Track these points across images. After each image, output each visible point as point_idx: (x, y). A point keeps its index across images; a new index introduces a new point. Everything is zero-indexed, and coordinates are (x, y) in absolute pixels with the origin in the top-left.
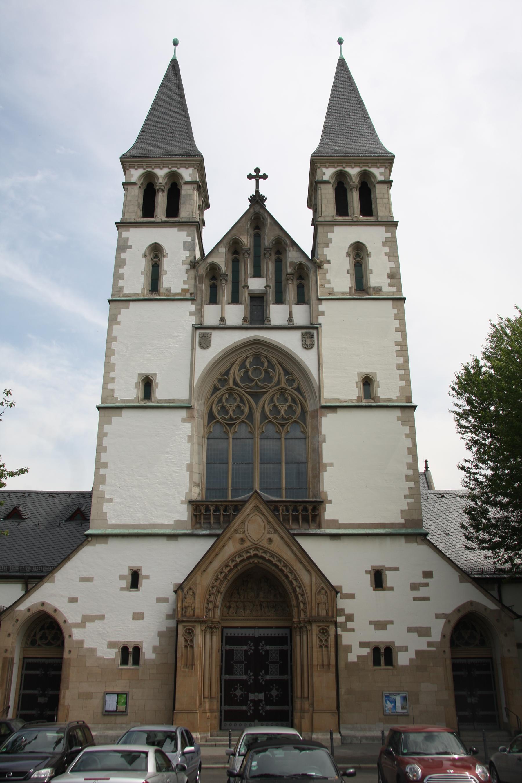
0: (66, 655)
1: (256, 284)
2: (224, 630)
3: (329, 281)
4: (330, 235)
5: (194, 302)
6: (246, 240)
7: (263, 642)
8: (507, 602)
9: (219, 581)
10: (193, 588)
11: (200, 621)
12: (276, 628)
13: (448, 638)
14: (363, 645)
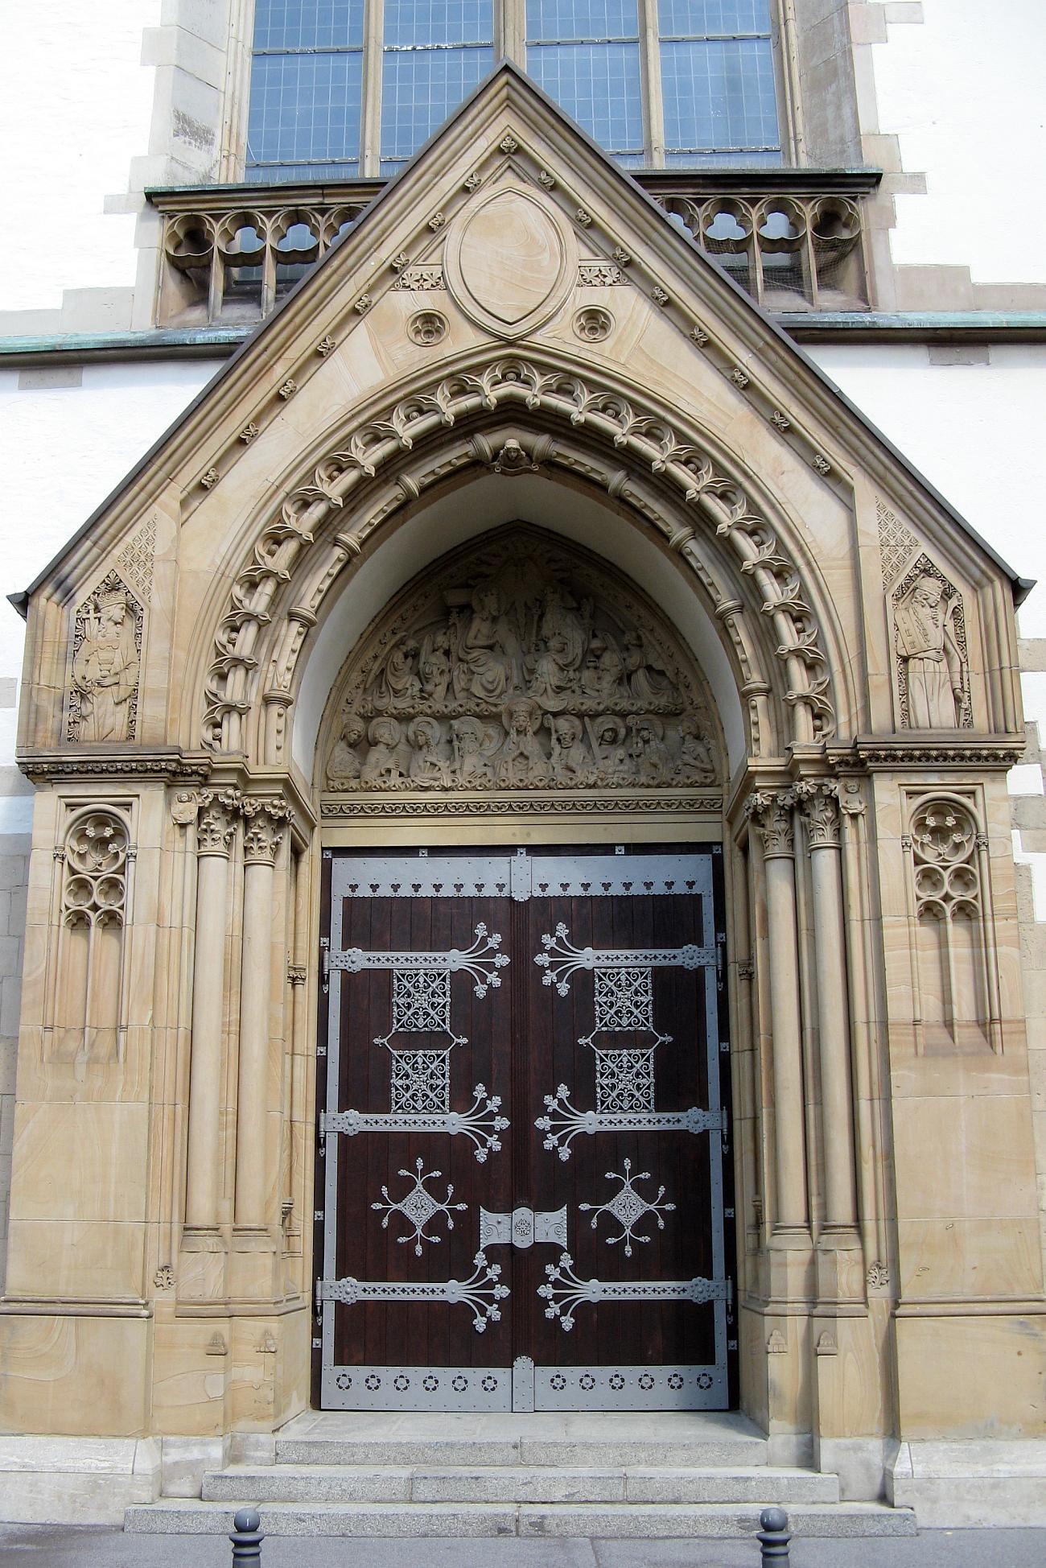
2: (339, 863)
7: (562, 930)
9: (290, 548)
10: (129, 581)
11: (175, 773)
12: (634, 849)
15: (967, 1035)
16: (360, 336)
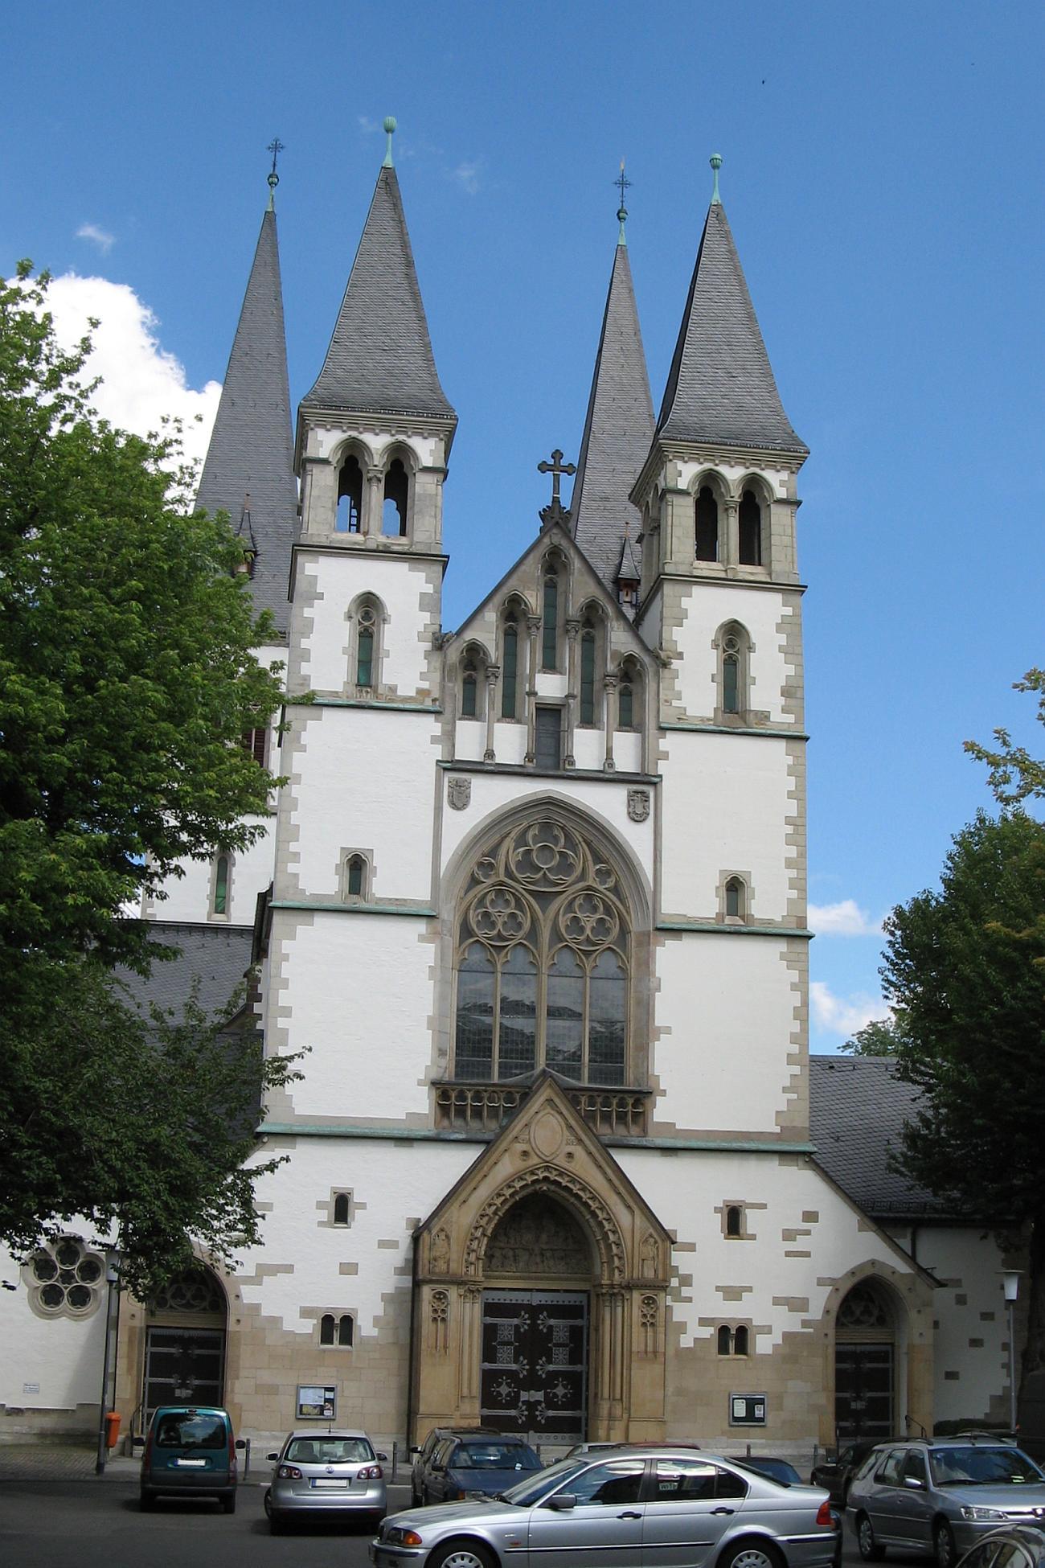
0: (232, 1326)
1: (550, 687)
3: (680, 693)
4: (685, 602)
5: (441, 717)
6: (534, 600)
8: (923, 1260)
11: (459, 1282)
13: (834, 1314)
14: (704, 1322)
15: (650, 1355)
16: (506, 1159)
